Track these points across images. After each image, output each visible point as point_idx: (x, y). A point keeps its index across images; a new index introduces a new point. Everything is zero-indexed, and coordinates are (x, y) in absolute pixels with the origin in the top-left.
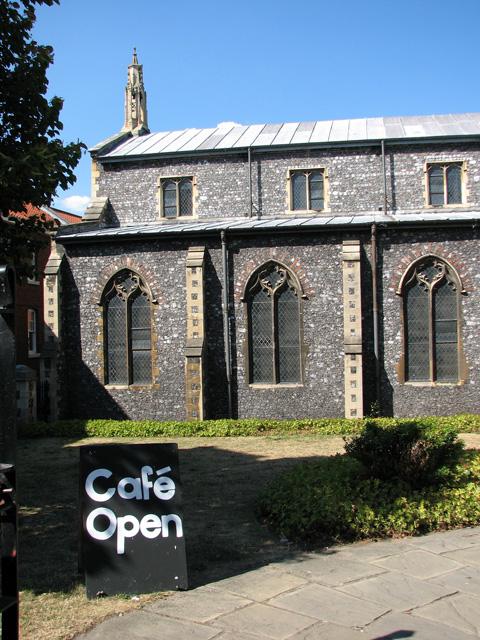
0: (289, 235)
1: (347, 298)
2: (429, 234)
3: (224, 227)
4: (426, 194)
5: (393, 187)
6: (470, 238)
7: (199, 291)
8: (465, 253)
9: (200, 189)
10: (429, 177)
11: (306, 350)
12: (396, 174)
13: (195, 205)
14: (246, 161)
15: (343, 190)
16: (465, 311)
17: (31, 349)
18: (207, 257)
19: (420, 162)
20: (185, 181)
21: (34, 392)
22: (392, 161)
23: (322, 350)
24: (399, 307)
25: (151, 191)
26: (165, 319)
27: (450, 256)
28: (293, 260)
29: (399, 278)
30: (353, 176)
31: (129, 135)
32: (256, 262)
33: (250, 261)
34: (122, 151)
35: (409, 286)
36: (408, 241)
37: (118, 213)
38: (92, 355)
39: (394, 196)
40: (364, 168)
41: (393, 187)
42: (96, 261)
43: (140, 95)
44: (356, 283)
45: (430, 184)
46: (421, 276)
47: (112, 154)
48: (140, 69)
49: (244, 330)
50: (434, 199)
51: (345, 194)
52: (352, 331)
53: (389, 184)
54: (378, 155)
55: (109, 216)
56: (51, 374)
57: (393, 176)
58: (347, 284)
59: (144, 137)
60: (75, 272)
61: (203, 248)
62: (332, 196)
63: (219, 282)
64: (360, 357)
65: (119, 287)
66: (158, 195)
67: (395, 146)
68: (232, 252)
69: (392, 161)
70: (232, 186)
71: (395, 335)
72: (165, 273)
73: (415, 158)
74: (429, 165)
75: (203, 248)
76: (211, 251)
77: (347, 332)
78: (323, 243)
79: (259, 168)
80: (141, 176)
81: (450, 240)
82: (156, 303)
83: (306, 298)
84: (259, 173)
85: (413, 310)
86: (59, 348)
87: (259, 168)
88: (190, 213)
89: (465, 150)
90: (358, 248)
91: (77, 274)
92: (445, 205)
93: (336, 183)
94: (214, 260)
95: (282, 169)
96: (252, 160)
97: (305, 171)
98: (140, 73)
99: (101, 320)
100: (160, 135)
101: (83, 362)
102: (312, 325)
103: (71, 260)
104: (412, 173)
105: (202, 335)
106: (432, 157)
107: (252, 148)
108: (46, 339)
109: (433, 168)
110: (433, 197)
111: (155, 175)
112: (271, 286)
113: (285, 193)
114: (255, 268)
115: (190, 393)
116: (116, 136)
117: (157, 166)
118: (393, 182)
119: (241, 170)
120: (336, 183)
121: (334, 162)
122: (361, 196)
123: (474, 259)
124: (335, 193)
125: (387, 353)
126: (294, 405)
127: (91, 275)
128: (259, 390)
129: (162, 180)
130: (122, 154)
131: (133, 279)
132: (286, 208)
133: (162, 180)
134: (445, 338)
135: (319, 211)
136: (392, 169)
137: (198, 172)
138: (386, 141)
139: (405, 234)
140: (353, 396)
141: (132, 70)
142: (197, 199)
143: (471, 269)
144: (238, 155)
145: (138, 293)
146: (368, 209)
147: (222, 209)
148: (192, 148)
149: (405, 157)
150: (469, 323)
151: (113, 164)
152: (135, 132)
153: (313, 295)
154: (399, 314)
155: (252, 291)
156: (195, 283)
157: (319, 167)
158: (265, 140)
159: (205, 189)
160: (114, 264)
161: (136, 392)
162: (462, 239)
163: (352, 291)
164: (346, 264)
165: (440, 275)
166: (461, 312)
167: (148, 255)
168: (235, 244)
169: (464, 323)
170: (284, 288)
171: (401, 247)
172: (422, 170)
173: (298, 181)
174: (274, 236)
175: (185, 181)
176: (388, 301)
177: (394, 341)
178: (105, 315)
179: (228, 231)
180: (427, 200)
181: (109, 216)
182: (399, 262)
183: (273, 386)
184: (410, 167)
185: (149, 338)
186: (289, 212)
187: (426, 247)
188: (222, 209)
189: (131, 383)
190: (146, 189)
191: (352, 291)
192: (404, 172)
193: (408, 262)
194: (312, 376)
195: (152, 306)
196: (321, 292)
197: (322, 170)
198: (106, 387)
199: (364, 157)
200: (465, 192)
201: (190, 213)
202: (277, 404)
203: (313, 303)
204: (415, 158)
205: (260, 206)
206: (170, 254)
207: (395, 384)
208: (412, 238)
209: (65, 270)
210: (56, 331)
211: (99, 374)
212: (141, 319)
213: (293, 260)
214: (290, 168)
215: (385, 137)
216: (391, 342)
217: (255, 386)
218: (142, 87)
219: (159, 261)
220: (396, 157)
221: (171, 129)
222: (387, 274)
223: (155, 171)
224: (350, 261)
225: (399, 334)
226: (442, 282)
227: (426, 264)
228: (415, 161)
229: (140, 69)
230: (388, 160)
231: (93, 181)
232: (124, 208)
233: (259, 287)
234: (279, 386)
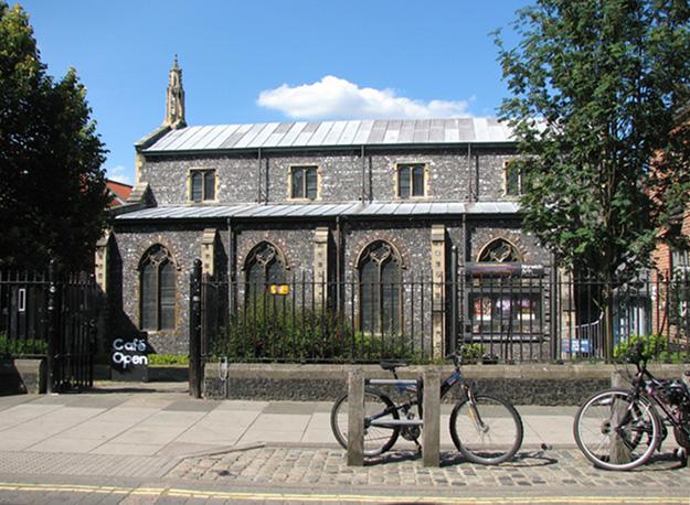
3: (230, 214)
4: (396, 188)
5: (371, 182)
6: (409, 228)
9: (221, 179)
10: (399, 174)
13: (217, 192)
14: (257, 158)
15: (332, 183)
17: (82, 303)
18: (217, 237)
20: (210, 172)
25: (182, 179)
31: (169, 129)
33: (249, 241)
34: (159, 146)
35: (364, 262)
36: (364, 228)
37: (156, 196)
38: (131, 307)
39: (371, 188)
40: (349, 167)
41: (371, 182)
42: (136, 237)
43: (180, 95)
45: (399, 180)
46: (373, 255)
47: (148, 150)
48: (180, 72)
49: (243, 292)
50: (402, 192)
53: (367, 180)
54: (360, 156)
57: (370, 173)
58: (317, 260)
59: (181, 131)
60: (119, 244)
62: (323, 188)
63: (226, 256)
65: (152, 257)
66: (188, 183)
68: (236, 233)
72: (187, 247)
76: (221, 232)
79: (267, 164)
80: (175, 167)
81: (394, 228)
84: (268, 168)
85: (366, 279)
87: (267, 164)
88: (213, 198)
90: (326, 233)
91: (121, 246)
92: (411, 197)
93: (327, 178)
94: (222, 239)
95: (284, 166)
96: (262, 158)
98: (180, 77)
99: (138, 281)
100: (195, 129)
103: (117, 236)
106: (401, 159)
107: (262, 149)
109: (401, 168)
111: (186, 166)
113: (287, 185)
114: (253, 245)
116: (158, 130)
119: (253, 165)
120: (327, 178)
127: (132, 248)
129: (191, 171)
130: (160, 149)
133: (191, 171)
135: (313, 199)
136: (371, 167)
137: (219, 166)
138: (365, 146)
139: (362, 224)
141: (173, 74)
142: (219, 187)
144: (251, 154)
145: (166, 261)
146: (352, 199)
147: (238, 196)
148: (215, 147)
151: (153, 157)
152: (173, 126)
155: (250, 263)
156: (208, 256)
157: (314, 164)
158: (273, 142)
159: (225, 180)
160: (149, 240)
161: (163, 336)
162: (404, 228)
165: (387, 254)
167: (174, 234)
170: (274, 260)
171: (359, 233)
173: (298, 175)
175: (210, 172)
176: (348, 273)
178: (141, 278)
179: (233, 218)
180: (397, 193)
181: (149, 200)
182: (357, 244)
184: (384, 167)
185: (174, 296)
186: (289, 199)
188: (238, 196)
190: (178, 178)
191: (321, 265)
192: (379, 171)
193: (363, 244)
195: (177, 272)
197: (316, 167)
199: (349, 158)
200: (427, 188)
201: (213, 198)
209: (112, 243)
210: (104, 289)
211: (136, 322)
212: (169, 282)
215: (364, 143)
218: (181, 88)
219: (182, 239)
220: (373, 159)
221: (205, 124)
222: (348, 253)
223: (186, 163)
226: (389, 259)
227: (377, 246)
229: (180, 72)
230: (367, 160)
231: (137, 169)
232: (161, 192)
233: (255, 260)
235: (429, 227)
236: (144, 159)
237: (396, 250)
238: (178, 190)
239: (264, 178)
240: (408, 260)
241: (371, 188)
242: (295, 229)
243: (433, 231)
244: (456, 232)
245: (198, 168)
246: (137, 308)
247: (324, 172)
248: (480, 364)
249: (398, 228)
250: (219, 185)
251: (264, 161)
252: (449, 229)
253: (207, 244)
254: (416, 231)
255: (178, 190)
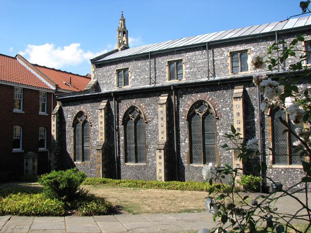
0: (139, 93)
1: (160, 122)
2: (200, 88)
4: (229, 68)
5: (214, 65)
7: (241, 110)
8: (217, 97)
9: (131, 73)
11: (147, 147)
12: (215, 59)
13: (130, 81)
15: (191, 69)
16: (218, 128)
19: (226, 51)
21: (36, 163)
22: (213, 52)
23: (154, 147)
24: (187, 126)
26: (94, 133)
27: (210, 99)
28: (141, 105)
29: (186, 111)
30: (195, 61)
31: (117, 51)
32: (127, 106)
33: (125, 105)
35: (191, 115)
36: (191, 93)
38: (70, 148)
39: (214, 70)
40: (200, 57)
41: (214, 65)
42: (72, 108)
43: (125, 32)
44: (164, 115)
45: (232, 62)
51: (192, 71)
52: (162, 138)
55: (97, 86)
56: (52, 156)
57: (214, 60)
61: (167, 95)
64: (163, 151)
66: (115, 77)
67: (214, 45)
69: (213, 52)
70: (144, 71)
71: (185, 140)
73: (224, 50)
74: (231, 53)
75: (167, 95)
77: (160, 139)
78: (154, 96)
79: (155, 61)
82: (91, 126)
83: (147, 123)
86: (56, 145)
87: (155, 61)
89: (248, 43)
93: (188, 66)
95: (163, 61)
97: (174, 61)
101: (67, 152)
102: (149, 136)
104: (223, 57)
105: (104, 140)
106: (232, 49)
108: (52, 142)
109: (232, 54)
110: (234, 68)
112: (201, 112)
115: (98, 166)
117: (115, 64)
118: (214, 63)
120: (188, 66)
121: (187, 55)
122: (199, 71)
123: (222, 100)
124: (187, 71)
125: (182, 150)
126: (143, 174)
127: (70, 112)
128: (129, 166)
131: (205, 105)
132: (166, 80)
133: (117, 70)
134: (210, 142)
136: (213, 56)
137: (130, 65)
139: (189, 90)
140: (160, 170)
143: (220, 106)
147: (140, 82)
149: (219, 49)
150: (220, 134)
152: (119, 49)
153: (150, 121)
154: (187, 130)
156: (101, 116)
157: (180, 58)
159: (133, 73)
163: (162, 119)
164: (160, 106)
165: (205, 109)
166: (216, 128)
168: (119, 98)
169: (217, 134)
171: (188, 96)
172: (227, 55)
174: (134, 94)
175: (126, 70)
177: (185, 143)
178: (75, 131)
181: (97, 86)
182: (186, 103)
183: (288, 166)
185: (89, 142)
186: (167, 81)
187: (199, 96)
188: (140, 82)
189: (83, 161)
191: (162, 119)
193: (190, 103)
194: (150, 160)
196: (153, 120)
197: (182, 60)
198: (75, 163)
202: (136, 173)
203: (150, 125)
204: (224, 50)
205: (155, 79)
206: (96, 104)
207: (186, 165)
208: (192, 91)
209: (60, 111)
211: (72, 157)
213: (141, 105)
214: (168, 60)
216: (183, 144)
217: (127, 164)
220: (215, 50)
222: (181, 110)
223: (114, 66)
224: (161, 104)
225: (187, 139)
227: (199, 104)
228: (224, 51)
232: (103, 84)
233: (195, 113)
234: (137, 164)
235: (233, 88)
236: (95, 66)
237: (211, 106)
238: (111, 82)
239: (153, 71)
240: (220, 113)
241: (214, 70)
242: (150, 97)
243: (235, 91)
244: (253, 90)
245: (120, 68)
246: (73, 149)
247: (186, 63)
248: (236, 207)
249: (213, 91)
250: (131, 76)
251: (152, 61)
252: (247, 89)
253: (101, 110)
254: (225, 91)
255: (111, 82)
